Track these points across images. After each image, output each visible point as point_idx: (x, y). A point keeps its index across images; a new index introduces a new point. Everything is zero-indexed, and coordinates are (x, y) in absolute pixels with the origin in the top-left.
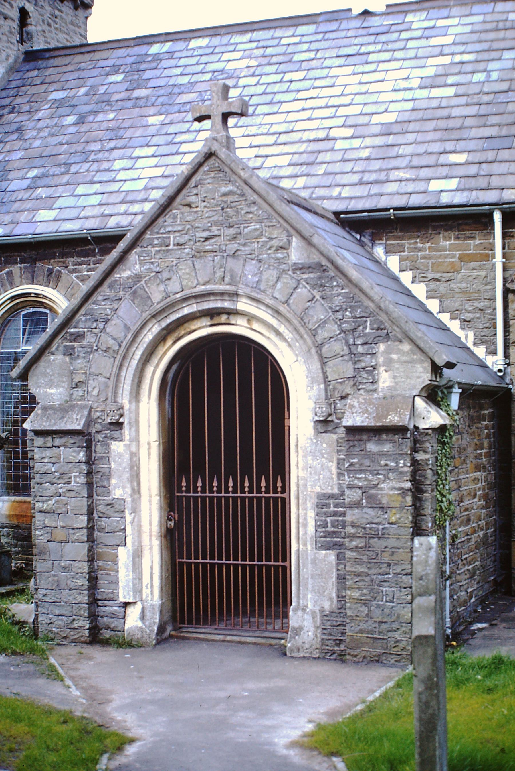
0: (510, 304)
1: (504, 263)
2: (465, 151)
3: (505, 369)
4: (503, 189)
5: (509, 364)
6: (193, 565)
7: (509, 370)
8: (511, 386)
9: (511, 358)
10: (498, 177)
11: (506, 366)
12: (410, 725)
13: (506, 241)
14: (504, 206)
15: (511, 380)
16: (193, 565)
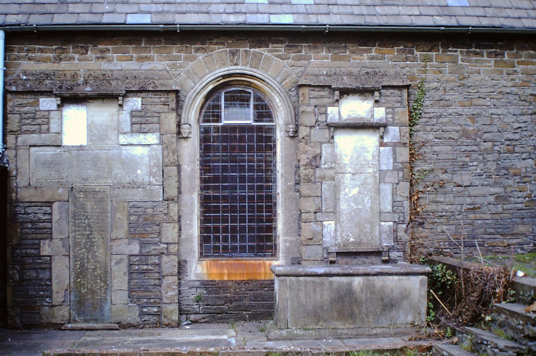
0: (8, 102)
1: (4, 71)
2: (70, 13)
3: (3, 152)
4: (7, 14)
5: (6, 149)
6: (221, 181)
7: (7, 152)
8: (7, 165)
9: (8, 144)
10: (4, 5)
11: (4, 150)
12: (45, 320)
13: (8, 54)
14: (7, 27)
15: (8, 160)
16: (221, 181)
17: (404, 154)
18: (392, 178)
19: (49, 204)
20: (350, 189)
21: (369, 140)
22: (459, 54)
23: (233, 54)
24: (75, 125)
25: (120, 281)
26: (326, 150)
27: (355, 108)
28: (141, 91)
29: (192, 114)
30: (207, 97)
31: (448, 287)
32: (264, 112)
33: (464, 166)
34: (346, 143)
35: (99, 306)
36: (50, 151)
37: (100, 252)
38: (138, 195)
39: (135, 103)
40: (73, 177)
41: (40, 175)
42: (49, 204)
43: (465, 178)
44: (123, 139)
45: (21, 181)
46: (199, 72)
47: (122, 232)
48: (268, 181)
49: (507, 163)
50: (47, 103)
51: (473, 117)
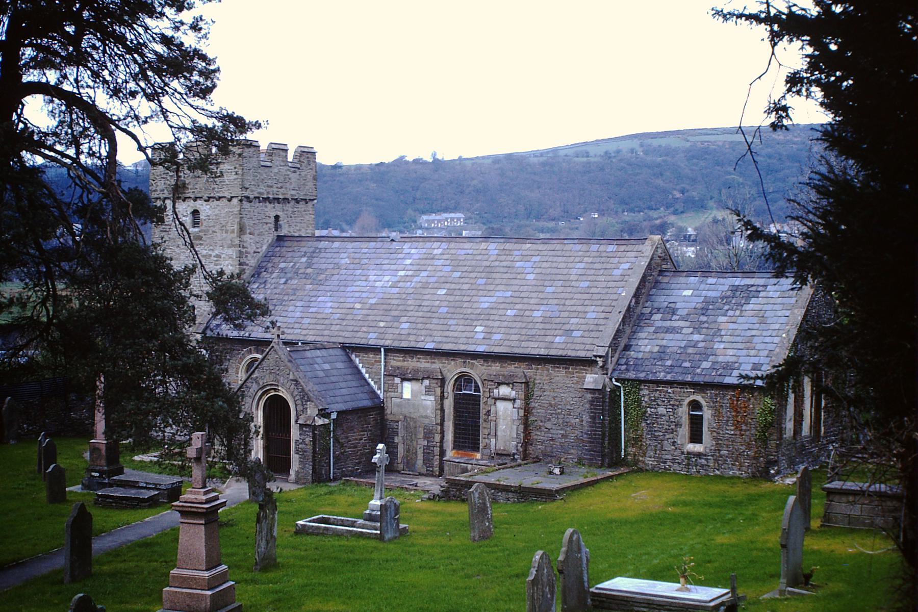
17: (522, 413)
18: (517, 423)
19: (398, 422)
20: (502, 427)
21: (509, 405)
22: (549, 367)
23: (464, 362)
24: (407, 390)
25: (420, 456)
26: (493, 408)
27: (505, 390)
28: (428, 378)
29: (449, 388)
30: (456, 380)
31: (8, 187)
32: (477, 389)
33: (549, 419)
34: (501, 405)
35: (414, 465)
36: (399, 400)
37: (415, 443)
38: (427, 421)
39: (426, 382)
40: (405, 411)
41: (395, 410)
42: (398, 422)
43: (548, 425)
44: (423, 398)
45: (388, 411)
46: (452, 370)
47: (421, 436)
48: (459, 416)
49: (567, 420)
50: (397, 380)
51: (554, 398)
